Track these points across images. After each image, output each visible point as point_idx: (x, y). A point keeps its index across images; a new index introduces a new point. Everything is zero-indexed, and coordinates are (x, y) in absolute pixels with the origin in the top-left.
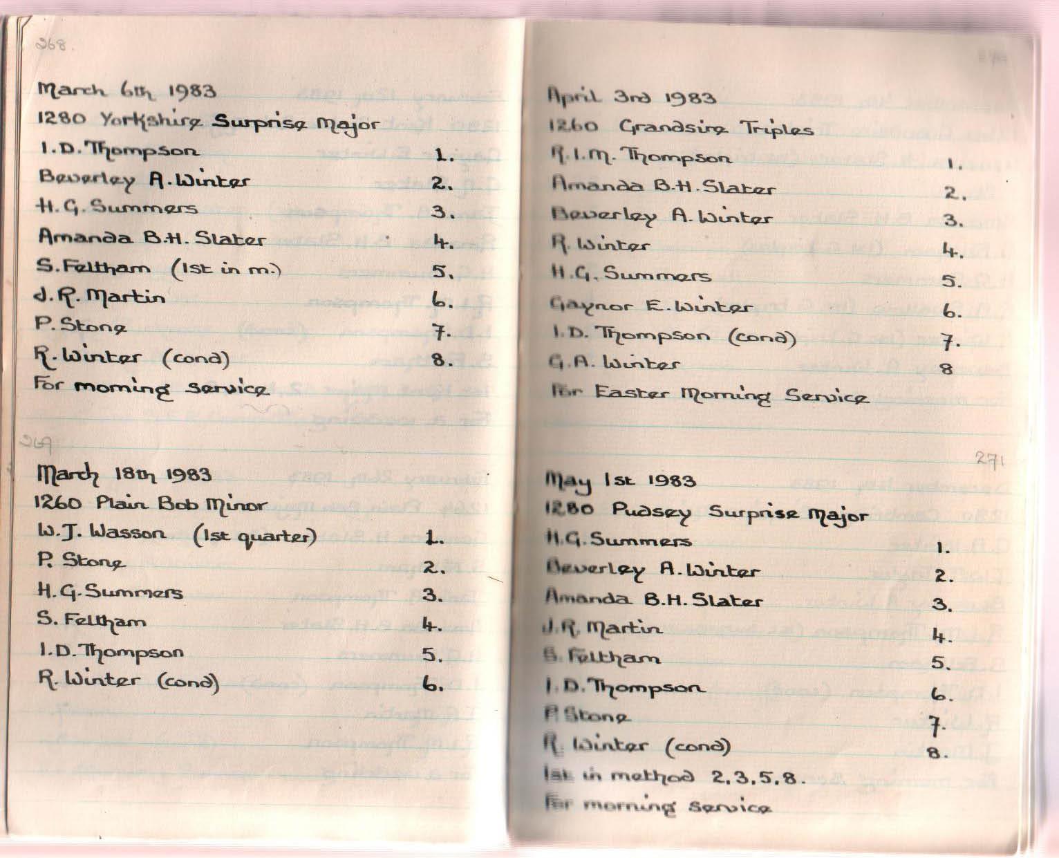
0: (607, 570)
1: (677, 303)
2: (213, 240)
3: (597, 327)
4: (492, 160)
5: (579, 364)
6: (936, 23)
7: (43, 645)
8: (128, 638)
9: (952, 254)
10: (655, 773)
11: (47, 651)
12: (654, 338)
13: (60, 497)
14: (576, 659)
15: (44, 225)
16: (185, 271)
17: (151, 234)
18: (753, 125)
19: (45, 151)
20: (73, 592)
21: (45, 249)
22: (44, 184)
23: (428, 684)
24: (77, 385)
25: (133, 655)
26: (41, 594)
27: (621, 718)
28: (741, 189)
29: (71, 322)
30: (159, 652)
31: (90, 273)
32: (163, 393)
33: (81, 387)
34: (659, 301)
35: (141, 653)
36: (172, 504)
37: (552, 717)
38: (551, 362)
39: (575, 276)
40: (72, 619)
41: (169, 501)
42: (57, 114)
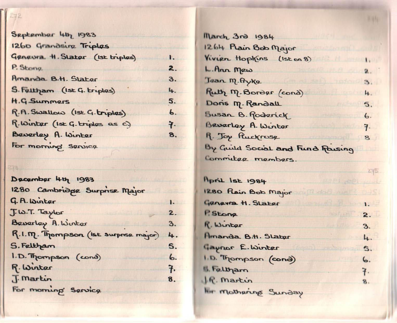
1: (251, 246)
2: (77, 79)
6: (352, 7)
7: (13, 254)
8: (47, 252)
9: (172, 91)
11: (15, 256)
12: (242, 260)
14: (215, 270)
17: (54, 78)
19: (13, 257)
20: (92, 113)
21: (15, 83)
23: (171, 257)
24: (29, 146)
26: (12, 102)
27: (267, 93)
28: (267, 204)
30: (253, 259)
31: (31, 93)
32: (60, 148)
33: (31, 146)
34: (245, 245)
36: (17, 223)
38: (205, 203)
40: (25, 245)
42: (19, 188)
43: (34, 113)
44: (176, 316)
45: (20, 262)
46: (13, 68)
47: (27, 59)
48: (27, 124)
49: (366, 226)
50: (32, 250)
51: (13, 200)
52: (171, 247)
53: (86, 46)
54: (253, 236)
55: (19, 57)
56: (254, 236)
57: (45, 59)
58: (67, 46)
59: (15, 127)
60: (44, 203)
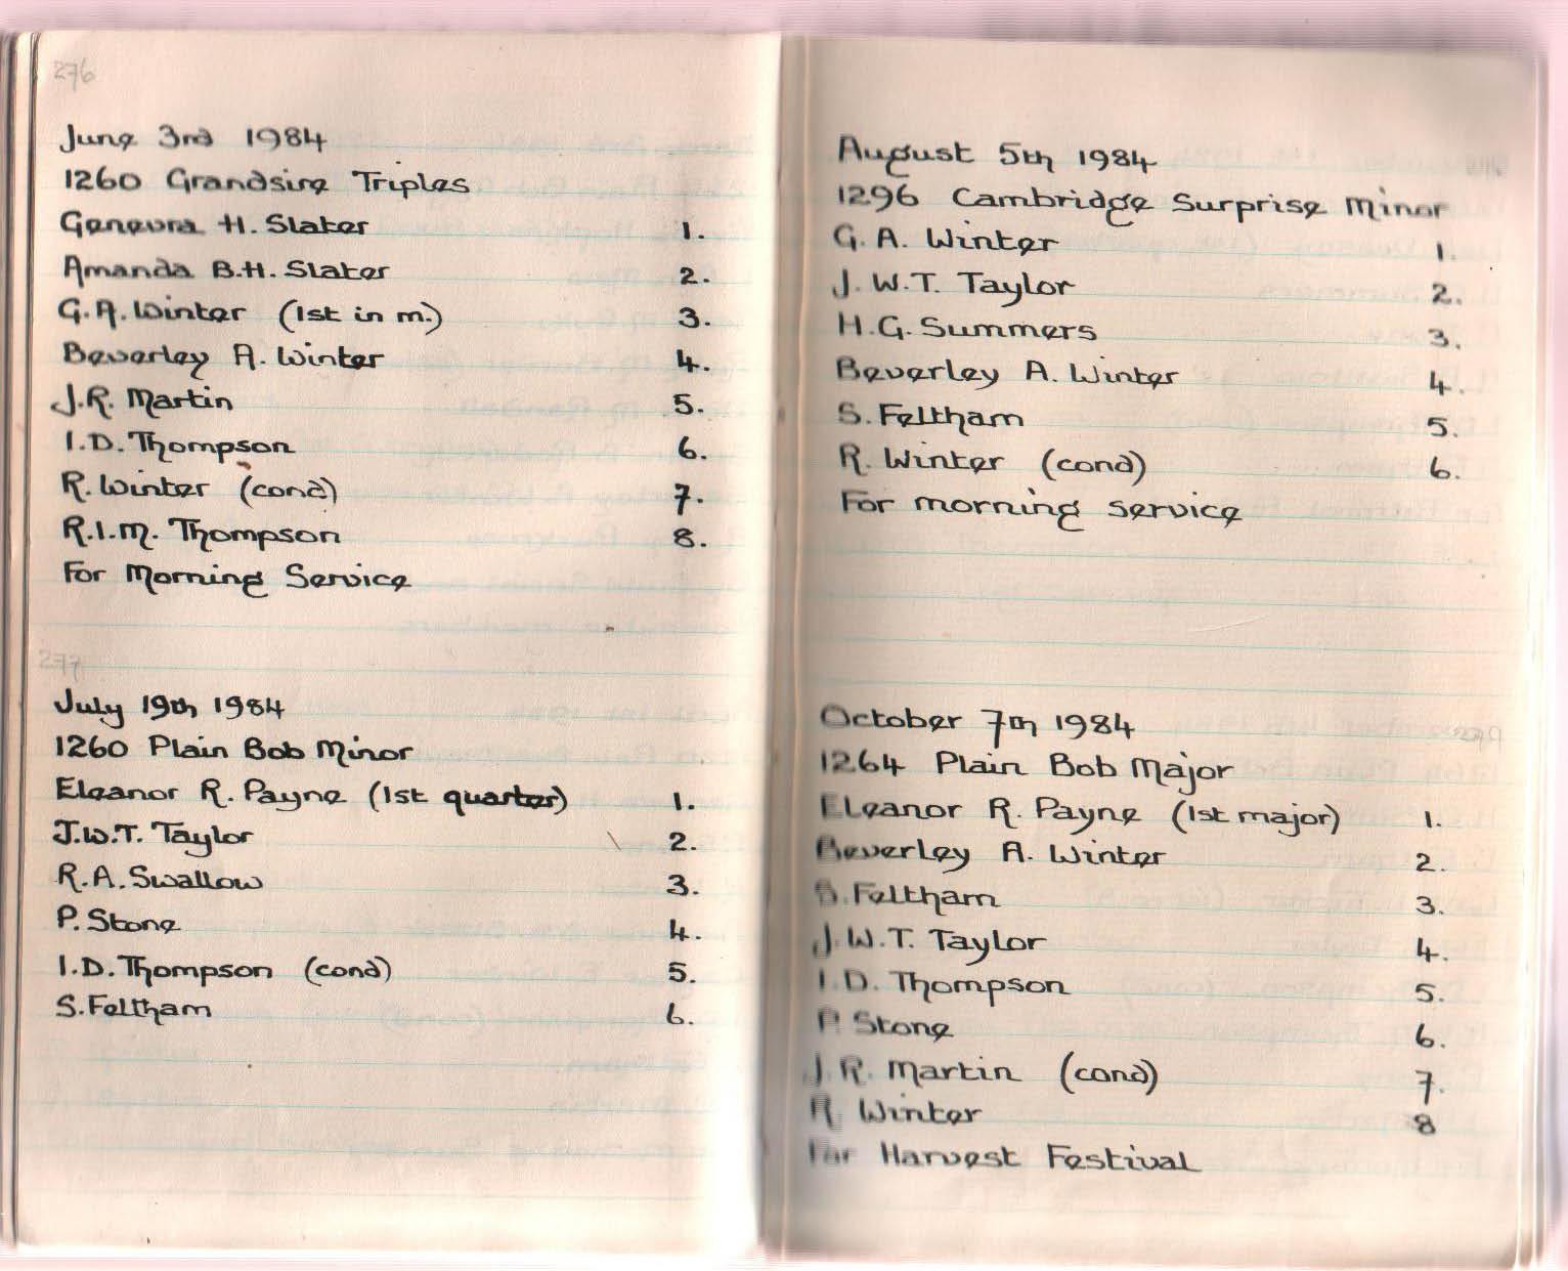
0: (914, 854)
3: (913, 275)
4: (726, 457)
5: (885, 242)
10: (1038, 154)
13: (102, 169)
15: (71, 252)
16: (300, 318)
18: (947, 939)
19: (63, 972)
22: (69, 365)
25: (196, 975)
29: (103, 916)
35: (208, 971)
36: (262, 751)
37: (830, 1028)
39: (877, 330)
41: (258, 746)
43: (143, 882)
44: (676, 1244)
45: (91, 464)
46: (61, 920)
47: (129, 235)
48: (126, 491)
49: (1428, 906)
50: (134, 944)
51: (70, 309)
52: (678, 976)
53: (376, 182)
54: (243, 269)
55: (94, 227)
56: (248, 268)
57: (202, 233)
58: (296, 185)
59: (75, 500)
60: (198, 319)
